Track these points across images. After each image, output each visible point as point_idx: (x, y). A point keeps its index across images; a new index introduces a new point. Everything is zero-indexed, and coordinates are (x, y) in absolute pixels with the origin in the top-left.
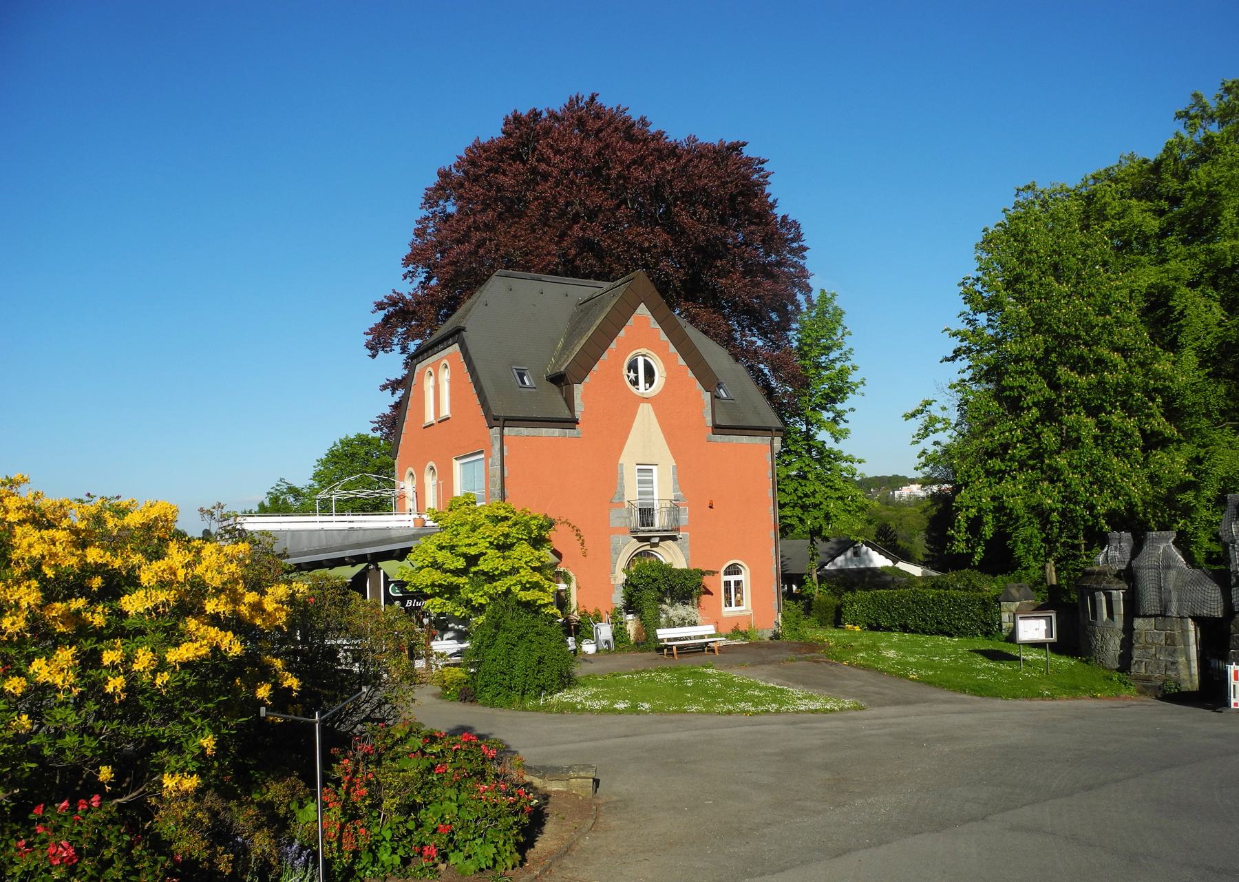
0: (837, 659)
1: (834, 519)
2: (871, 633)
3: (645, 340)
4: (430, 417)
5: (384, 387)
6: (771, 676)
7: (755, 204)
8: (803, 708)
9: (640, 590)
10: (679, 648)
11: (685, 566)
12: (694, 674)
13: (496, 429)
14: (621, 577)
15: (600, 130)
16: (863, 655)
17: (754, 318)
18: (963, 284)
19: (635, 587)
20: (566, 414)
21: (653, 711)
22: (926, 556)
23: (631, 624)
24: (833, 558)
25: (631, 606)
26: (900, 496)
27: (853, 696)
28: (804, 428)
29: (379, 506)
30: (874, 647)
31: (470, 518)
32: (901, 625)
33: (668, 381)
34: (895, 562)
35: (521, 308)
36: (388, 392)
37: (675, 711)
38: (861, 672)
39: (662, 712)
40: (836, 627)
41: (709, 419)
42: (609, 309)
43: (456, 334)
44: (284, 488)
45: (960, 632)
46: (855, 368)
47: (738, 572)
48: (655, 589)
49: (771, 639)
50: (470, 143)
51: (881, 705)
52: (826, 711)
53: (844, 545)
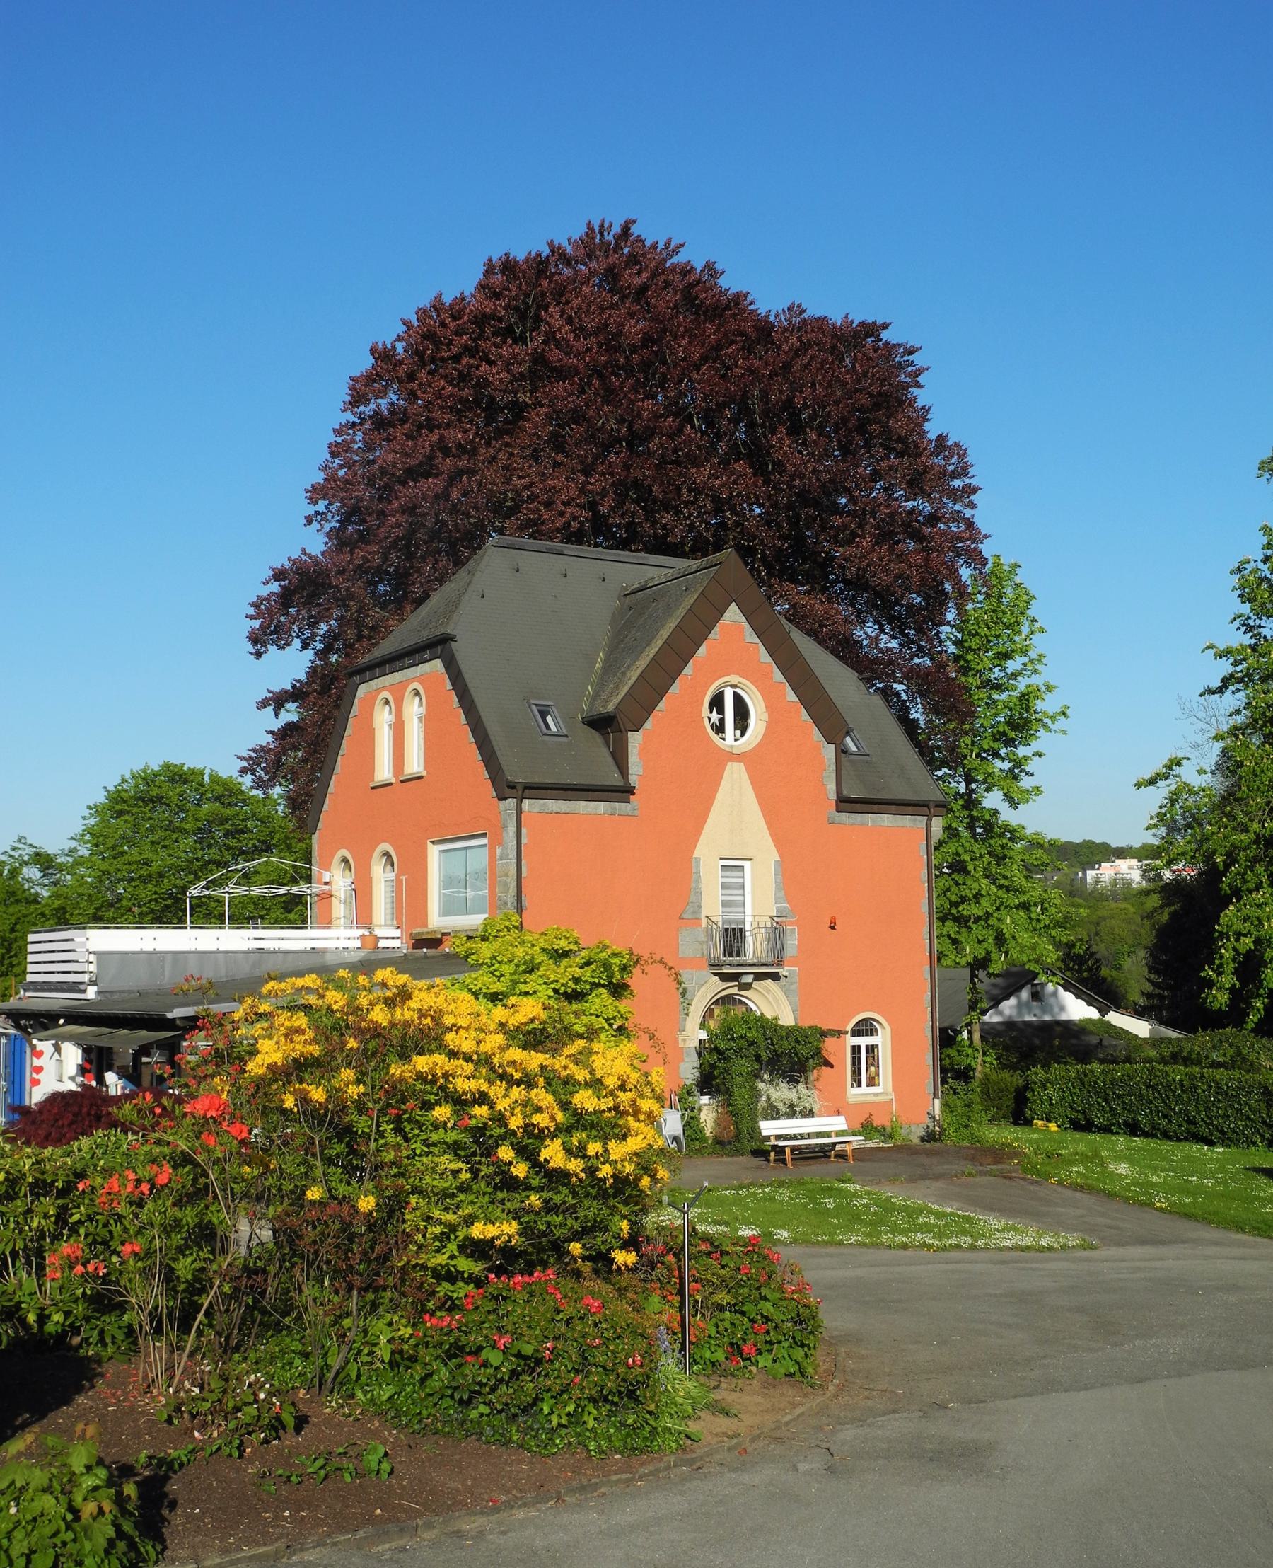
0: (1039, 1175)
1: (1012, 943)
2: (1078, 1135)
3: (735, 659)
4: (383, 772)
5: (263, 704)
6: (943, 1198)
7: (897, 425)
8: (1008, 1243)
9: (728, 1059)
10: (793, 1149)
11: (793, 1023)
12: (829, 1191)
13: (511, 803)
14: (694, 1034)
15: (643, 290)
16: (1081, 1169)
17: (883, 606)
18: (1239, 570)
19: (720, 1053)
20: (615, 779)
21: (795, 1241)
22: (1149, 996)
23: (708, 1112)
24: (996, 1002)
25: (708, 1082)
26: (1097, 881)
27: (1076, 1231)
28: (962, 788)
29: (292, 911)
30: (1094, 1158)
31: (520, 952)
32: (1126, 1124)
33: (771, 726)
34: (1103, 1012)
35: (536, 600)
36: (270, 710)
37: (827, 1243)
38: (1078, 1195)
39: (808, 1243)
40: (1015, 1123)
41: (832, 787)
42: (681, 612)
43: (439, 646)
44: (26, 853)
45: (1225, 1138)
46: (1049, 689)
47: (871, 1032)
48: (751, 1058)
49: (922, 1139)
50: (425, 301)
51: (1119, 1244)
52: (1041, 1249)
53: (1017, 980)
